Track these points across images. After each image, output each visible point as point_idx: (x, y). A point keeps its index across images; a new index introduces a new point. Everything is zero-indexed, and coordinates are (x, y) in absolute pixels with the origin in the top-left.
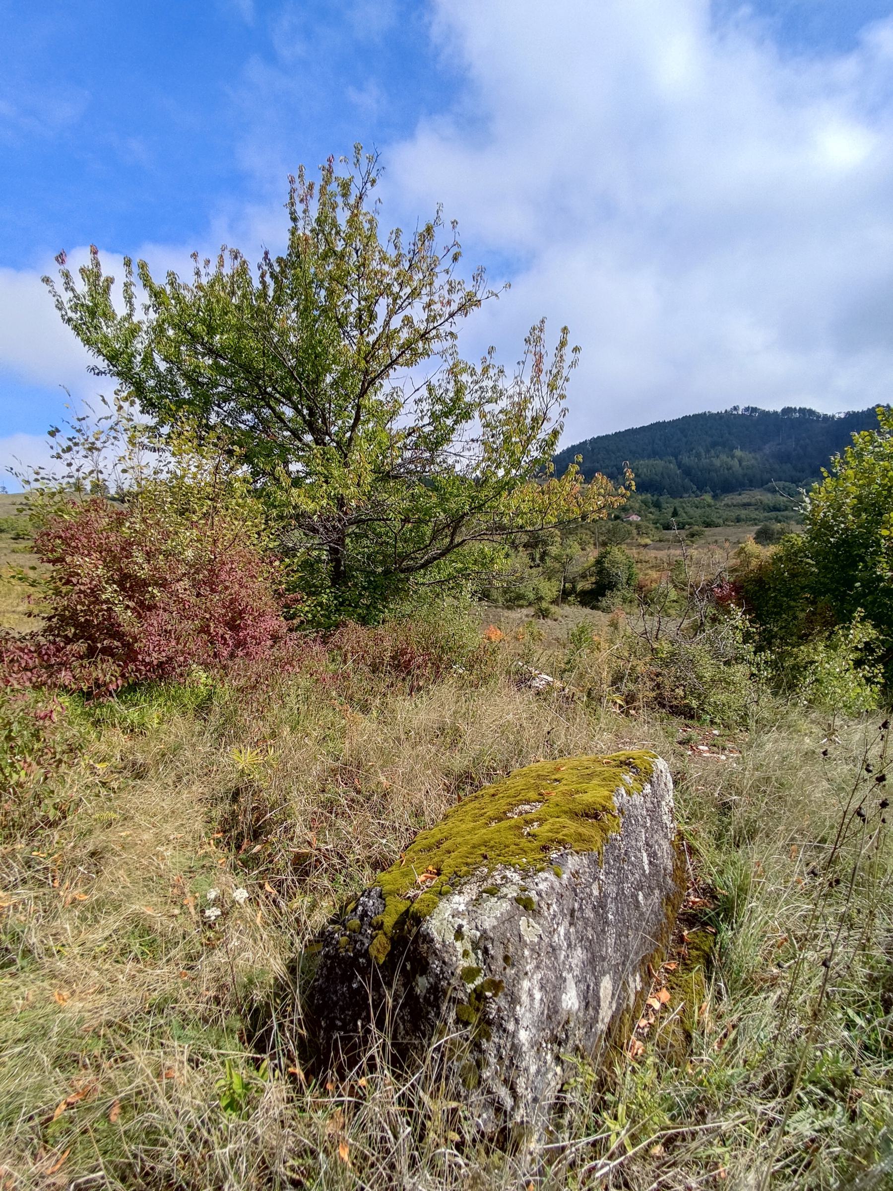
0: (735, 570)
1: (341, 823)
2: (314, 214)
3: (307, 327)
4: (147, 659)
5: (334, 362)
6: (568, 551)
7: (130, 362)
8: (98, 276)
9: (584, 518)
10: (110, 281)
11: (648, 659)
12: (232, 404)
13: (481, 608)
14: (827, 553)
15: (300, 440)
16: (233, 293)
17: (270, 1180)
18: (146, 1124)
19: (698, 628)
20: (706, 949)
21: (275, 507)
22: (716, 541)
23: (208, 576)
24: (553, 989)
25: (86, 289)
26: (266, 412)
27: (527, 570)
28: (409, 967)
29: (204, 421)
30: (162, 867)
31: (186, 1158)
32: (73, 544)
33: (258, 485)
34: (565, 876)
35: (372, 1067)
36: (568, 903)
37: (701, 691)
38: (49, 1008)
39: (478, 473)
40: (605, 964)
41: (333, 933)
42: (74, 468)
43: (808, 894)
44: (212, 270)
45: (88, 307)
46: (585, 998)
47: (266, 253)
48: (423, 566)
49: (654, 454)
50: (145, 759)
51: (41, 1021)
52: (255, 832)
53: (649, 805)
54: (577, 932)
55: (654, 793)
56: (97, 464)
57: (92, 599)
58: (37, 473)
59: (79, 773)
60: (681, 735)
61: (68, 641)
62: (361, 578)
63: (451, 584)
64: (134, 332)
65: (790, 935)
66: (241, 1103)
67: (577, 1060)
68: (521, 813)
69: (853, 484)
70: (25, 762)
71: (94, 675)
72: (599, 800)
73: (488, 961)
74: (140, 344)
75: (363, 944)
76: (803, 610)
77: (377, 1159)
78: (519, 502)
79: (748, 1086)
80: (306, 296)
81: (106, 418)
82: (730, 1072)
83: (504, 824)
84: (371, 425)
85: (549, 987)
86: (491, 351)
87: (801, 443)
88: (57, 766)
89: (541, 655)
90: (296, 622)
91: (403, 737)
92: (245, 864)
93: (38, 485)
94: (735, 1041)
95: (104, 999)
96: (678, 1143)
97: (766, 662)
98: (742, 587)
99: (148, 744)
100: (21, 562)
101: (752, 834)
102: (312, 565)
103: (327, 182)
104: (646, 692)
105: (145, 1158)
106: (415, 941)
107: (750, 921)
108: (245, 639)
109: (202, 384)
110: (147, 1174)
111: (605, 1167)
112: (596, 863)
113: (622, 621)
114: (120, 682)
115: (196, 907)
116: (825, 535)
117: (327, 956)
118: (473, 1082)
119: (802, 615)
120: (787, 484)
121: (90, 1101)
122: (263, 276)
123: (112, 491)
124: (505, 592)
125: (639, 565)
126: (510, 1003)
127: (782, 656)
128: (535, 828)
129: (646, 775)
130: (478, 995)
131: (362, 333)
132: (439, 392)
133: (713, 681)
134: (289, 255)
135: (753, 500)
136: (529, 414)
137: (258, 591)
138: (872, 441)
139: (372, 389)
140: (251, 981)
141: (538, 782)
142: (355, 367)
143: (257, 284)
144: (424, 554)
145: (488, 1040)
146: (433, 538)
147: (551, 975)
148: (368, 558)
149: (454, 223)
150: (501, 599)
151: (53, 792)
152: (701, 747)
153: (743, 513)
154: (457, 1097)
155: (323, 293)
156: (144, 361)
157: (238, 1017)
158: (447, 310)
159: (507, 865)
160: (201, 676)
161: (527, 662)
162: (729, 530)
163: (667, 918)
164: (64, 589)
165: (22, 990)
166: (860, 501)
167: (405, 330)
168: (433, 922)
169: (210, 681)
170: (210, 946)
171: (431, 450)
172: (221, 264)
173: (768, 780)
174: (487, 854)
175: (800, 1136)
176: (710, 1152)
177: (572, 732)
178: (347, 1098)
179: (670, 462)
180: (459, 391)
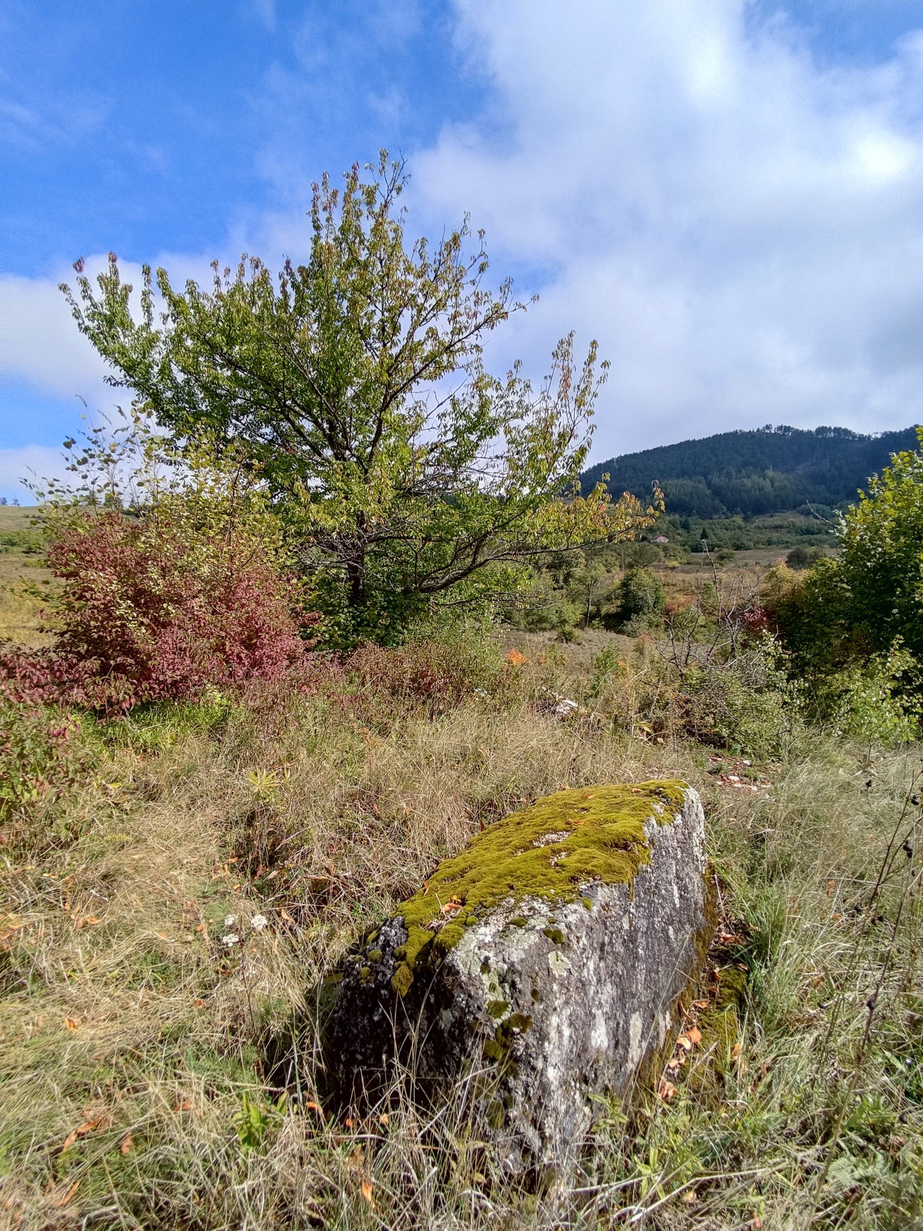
0: (766, 595)
1: (360, 850)
2: (338, 222)
3: (329, 338)
4: (161, 678)
5: (355, 375)
6: (593, 573)
7: (148, 372)
8: (116, 284)
9: (611, 538)
10: (128, 289)
11: (676, 685)
12: (251, 417)
13: (503, 630)
14: (864, 578)
15: (320, 455)
16: (254, 303)
17: (289, 1219)
18: (161, 1157)
19: (727, 655)
20: (739, 987)
21: (293, 523)
22: (746, 565)
23: (224, 593)
24: (582, 1025)
25: (104, 297)
26: (285, 425)
27: (551, 592)
28: (432, 1000)
29: (222, 434)
30: (176, 891)
31: (201, 1193)
32: (88, 558)
33: (275, 501)
34: (595, 908)
35: (395, 1104)
36: (598, 937)
37: (732, 719)
38: (59, 1035)
39: (503, 491)
40: (635, 1001)
41: (354, 963)
42: (89, 480)
43: (846, 932)
44: (233, 279)
45: (105, 315)
46: (615, 1036)
47: (288, 262)
48: (445, 586)
49: (683, 474)
50: (158, 780)
51: (52, 1048)
52: (271, 857)
53: (680, 836)
54: (607, 967)
55: (685, 824)
56: (112, 476)
57: (106, 615)
58: (52, 486)
59: (91, 794)
60: (711, 765)
61: (81, 657)
62: (380, 597)
63: (471, 605)
64: (152, 342)
65: (827, 975)
66: (258, 1137)
67: (607, 1102)
68: (547, 843)
69: (892, 507)
70: (37, 780)
71: (107, 692)
72: (629, 830)
73: (516, 995)
74: (157, 355)
75: (385, 975)
76: (838, 637)
77: (400, 1200)
78: (543, 522)
79: (785, 1132)
80: (328, 307)
81: (123, 430)
82: (766, 1116)
83: (531, 853)
84: (393, 440)
85: (578, 1024)
86: (517, 364)
87: (837, 464)
88: (70, 786)
89: (564, 680)
90: (313, 641)
91: (423, 762)
92: (260, 890)
93: (52, 498)
94: (769, 1085)
95: (116, 1026)
96: (712, 1190)
97: (799, 690)
98: (774, 612)
99: (161, 764)
100: (33, 577)
101: (787, 868)
102: (329, 584)
103: (351, 190)
104: (674, 721)
105: (159, 1192)
106: (440, 973)
107: (785, 960)
108: (261, 658)
109: (220, 396)
110: (161, 1209)
111: (638, 1212)
112: (627, 895)
113: (650, 647)
114: (133, 700)
115: (210, 933)
116: (862, 559)
117: (347, 987)
118: (500, 1121)
119: (836, 642)
120: (821, 506)
121: (101, 1131)
122: (284, 285)
123: (126, 506)
124: (527, 615)
125: (666, 589)
126: (538, 1040)
127: (815, 684)
128: (563, 858)
129: (677, 805)
130: (505, 1030)
131: (385, 345)
132: (463, 407)
133: (744, 708)
134: (312, 264)
135: (785, 523)
136: (556, 431)
137: (275, 609)
138: (912, 462)
139: (394, 403)
140: (268, 1012)
141: (565, 811)
142: (377, 380)
143: (278, 294)
144: (446, 574)
145: (515, 1078)
146: (455, 557)
147: (581, 1011)
148: (388, 577)
149: (481, 233)
150: (523, 622)
151: (64, 812)
152: (732, 778)
153: (775, 536)
154: (484, 1137)
155: (345, 304)
156: (161, 372)
157: (255, 1049)
158: (473, 322)
159: (535, 896)
160: (216, 696)
161: (551, 687)
162: (759, 553)
163: (698, 954)
164: (77, 605)
165: (25, 1015)
166: (899, 524)
167: (430, 342)
168: (459, 953)
169: (225, 701)
170: (226, 973)
171: (455, 467)
172: (242, 274)
173: (802, 813)
174: (513, 884)
175: (840, 1187)
176: (744, 1201)
177: (599, 759)
178: (369, 1135)
179: (699, 482)
180: (484, 405)
